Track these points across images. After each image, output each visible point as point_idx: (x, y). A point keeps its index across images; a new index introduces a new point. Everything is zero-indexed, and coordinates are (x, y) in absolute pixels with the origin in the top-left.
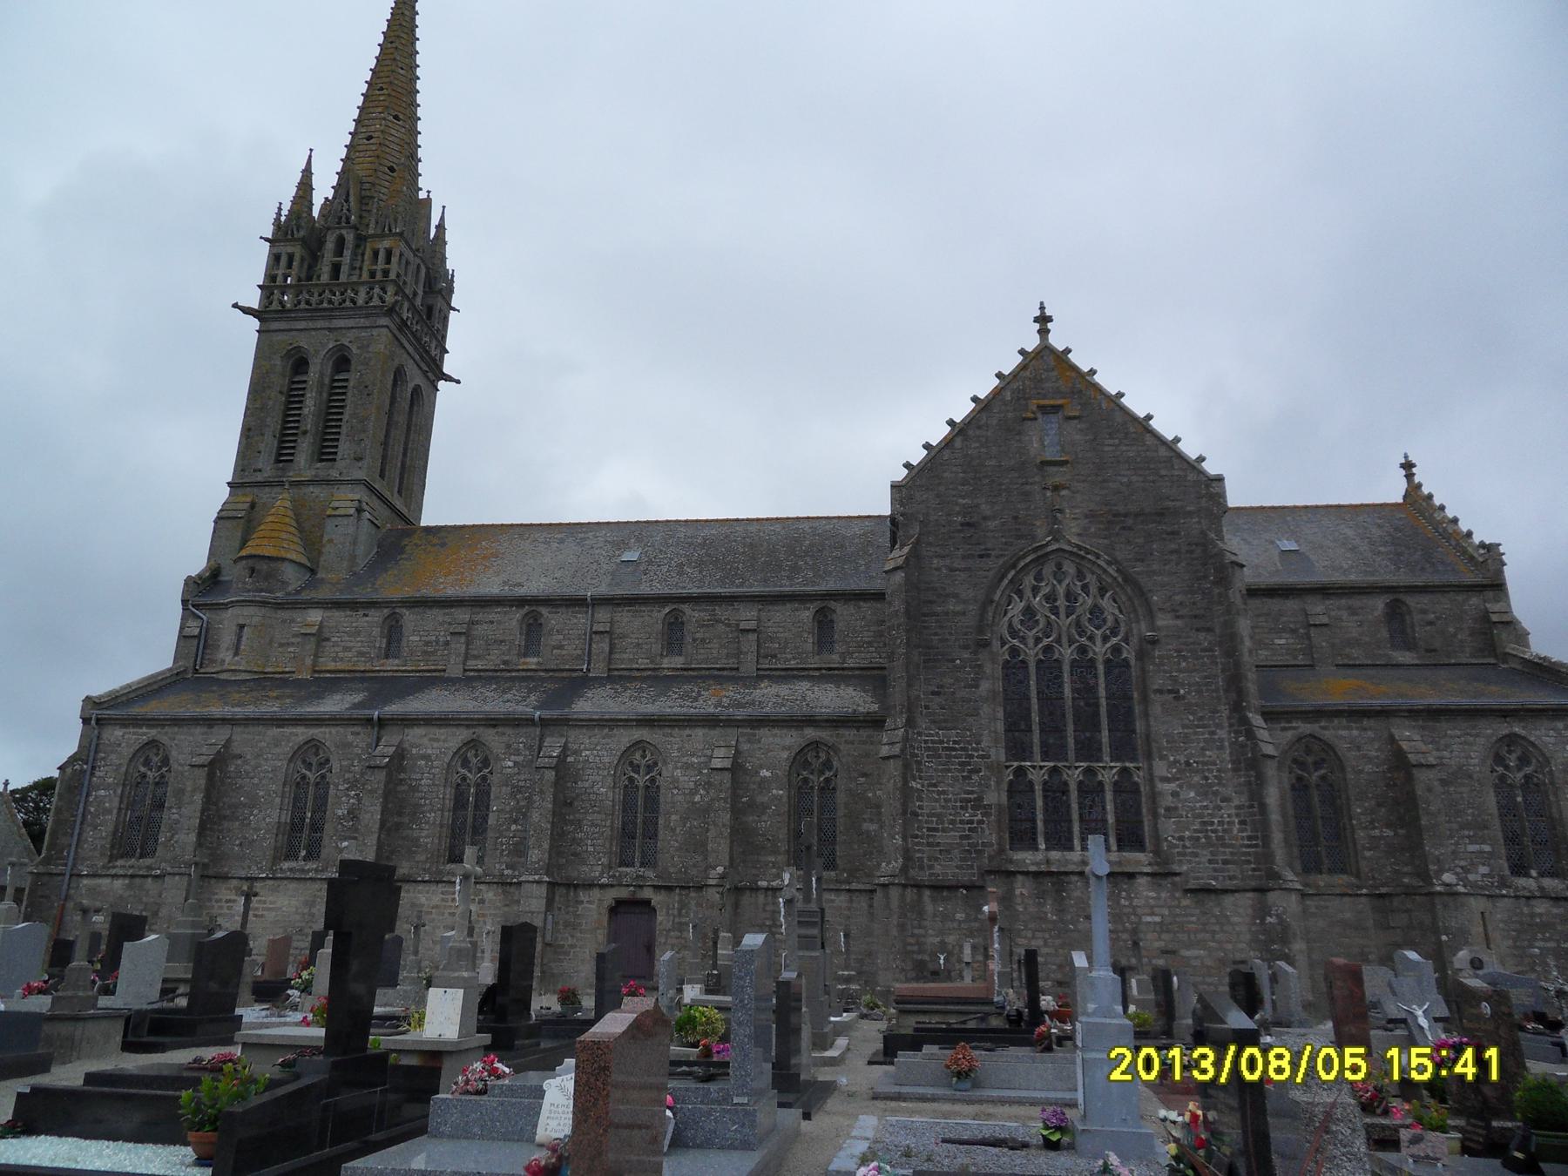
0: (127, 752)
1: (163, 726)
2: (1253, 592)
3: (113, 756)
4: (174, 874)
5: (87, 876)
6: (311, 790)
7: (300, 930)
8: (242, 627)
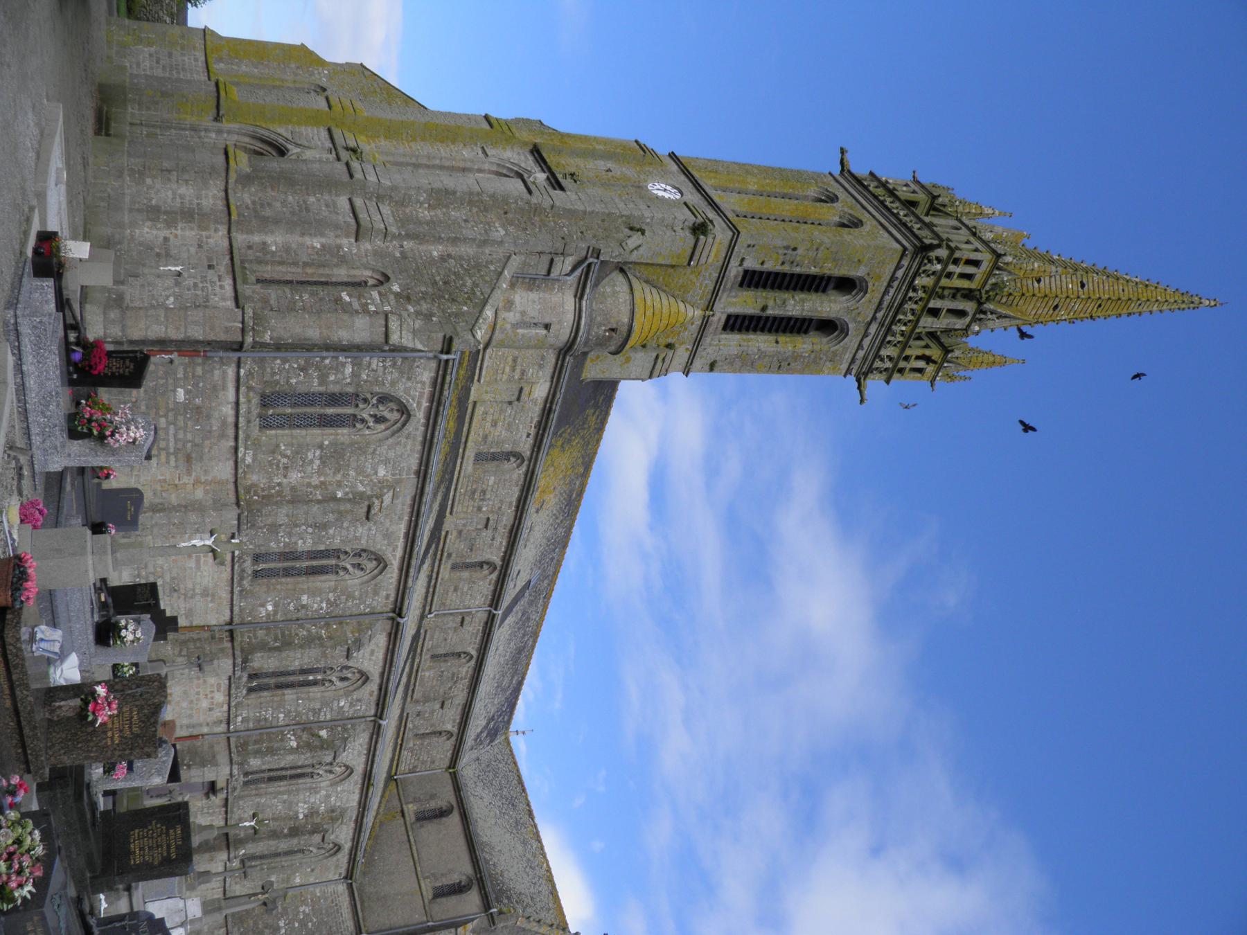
0: (400, 391)
2: (434, 657)
4: (239, 519)
5: (238, 373)
6: (333, 562)
7: (175, 591)
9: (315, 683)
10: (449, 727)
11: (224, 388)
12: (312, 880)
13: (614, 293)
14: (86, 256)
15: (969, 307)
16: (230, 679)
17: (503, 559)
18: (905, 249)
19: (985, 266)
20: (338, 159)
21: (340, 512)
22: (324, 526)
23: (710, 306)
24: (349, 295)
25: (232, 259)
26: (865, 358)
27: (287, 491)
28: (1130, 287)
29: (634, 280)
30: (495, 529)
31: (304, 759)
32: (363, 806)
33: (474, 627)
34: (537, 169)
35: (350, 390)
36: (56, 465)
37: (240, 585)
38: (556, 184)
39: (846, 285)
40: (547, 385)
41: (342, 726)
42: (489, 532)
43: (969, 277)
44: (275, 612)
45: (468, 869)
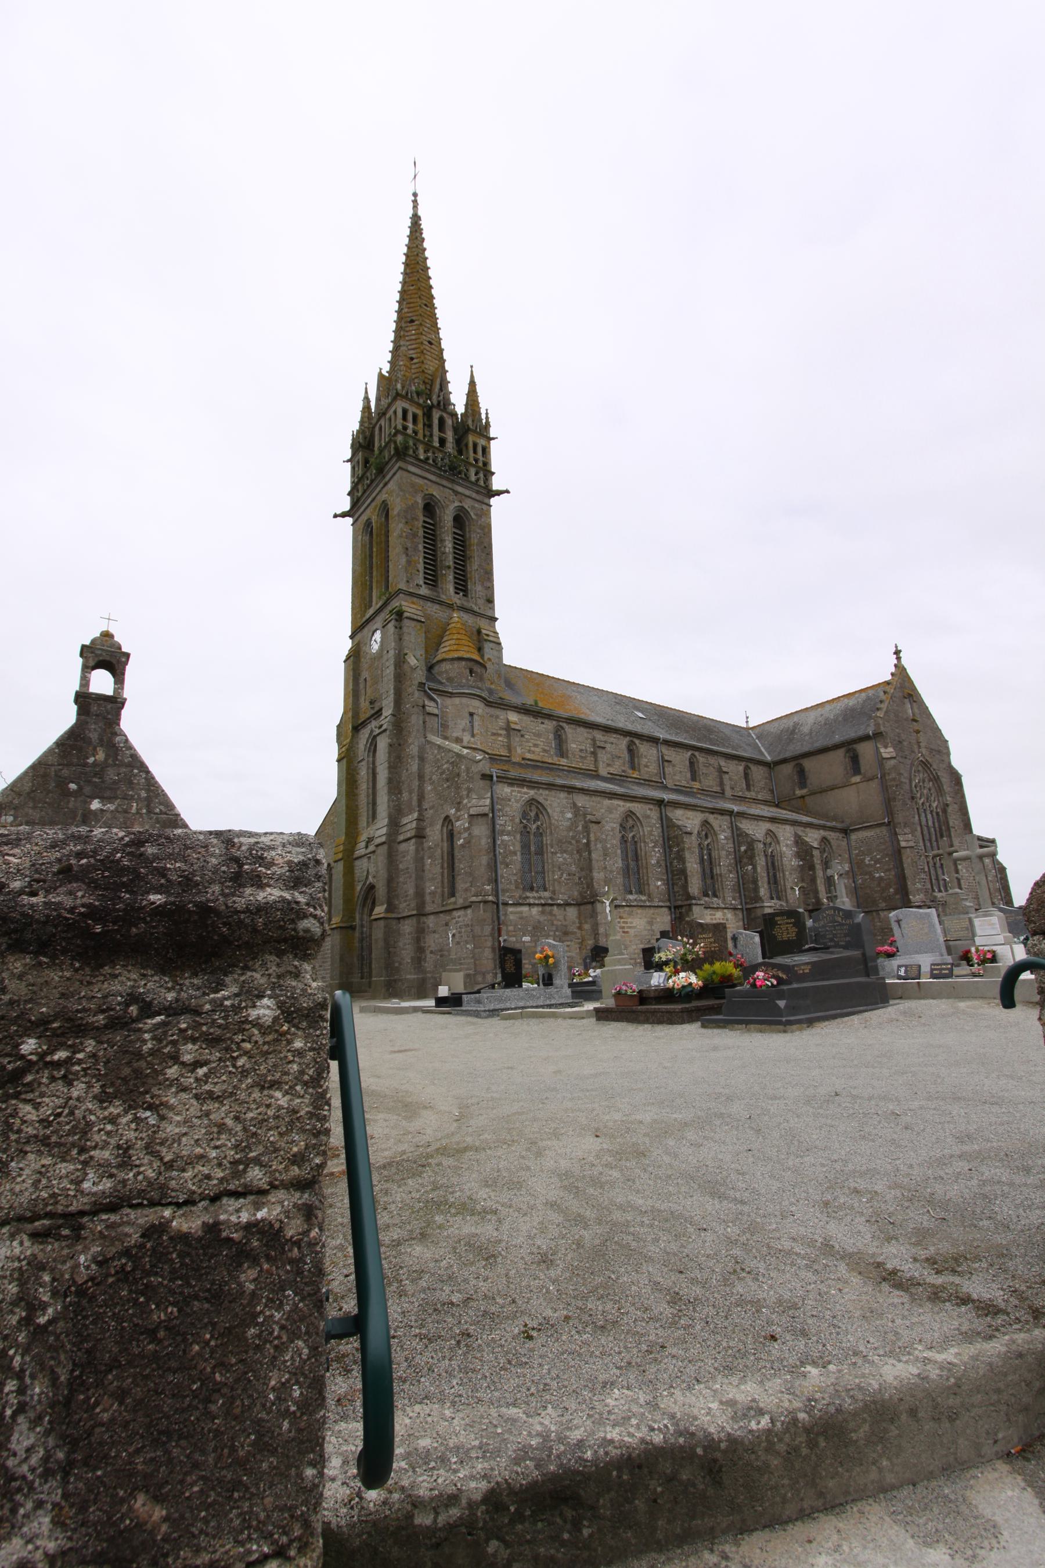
1: (539, 788)
2: (694, 778)
3: (508, 809)
8: (471, 714)
9: (710, 855)
10: (741, 768)
11: (521, 912)
12: (847, 856)
13: (446, 671)
14: (447, 988)
15: (436, 415)
16: (706, 908)
17: (625, 736)
18: (400, 468)
19: (407, 405)
20: (374, 852)
21: (596, 840)
22: (605, 849)
23: (450, 606)
24: (460, 839)
25: (441, 912)
26: (478, 492)
27: (583, 873)
28: (434, 397)
29: (439, 657)
30: (605, 742)
31: (761, 862)
32: (794, 823)
33: (669, 753)
34: (369, 727)
35: (518, 836)
36: (568, 991)
37: (644, 901)
38: (379, 713)
39: (430, 508)
40: (509, 712)
41: (738, 836)
42: (608, 746)
43: (415, 417)
44: (661, 880)
45: (841, 752)
